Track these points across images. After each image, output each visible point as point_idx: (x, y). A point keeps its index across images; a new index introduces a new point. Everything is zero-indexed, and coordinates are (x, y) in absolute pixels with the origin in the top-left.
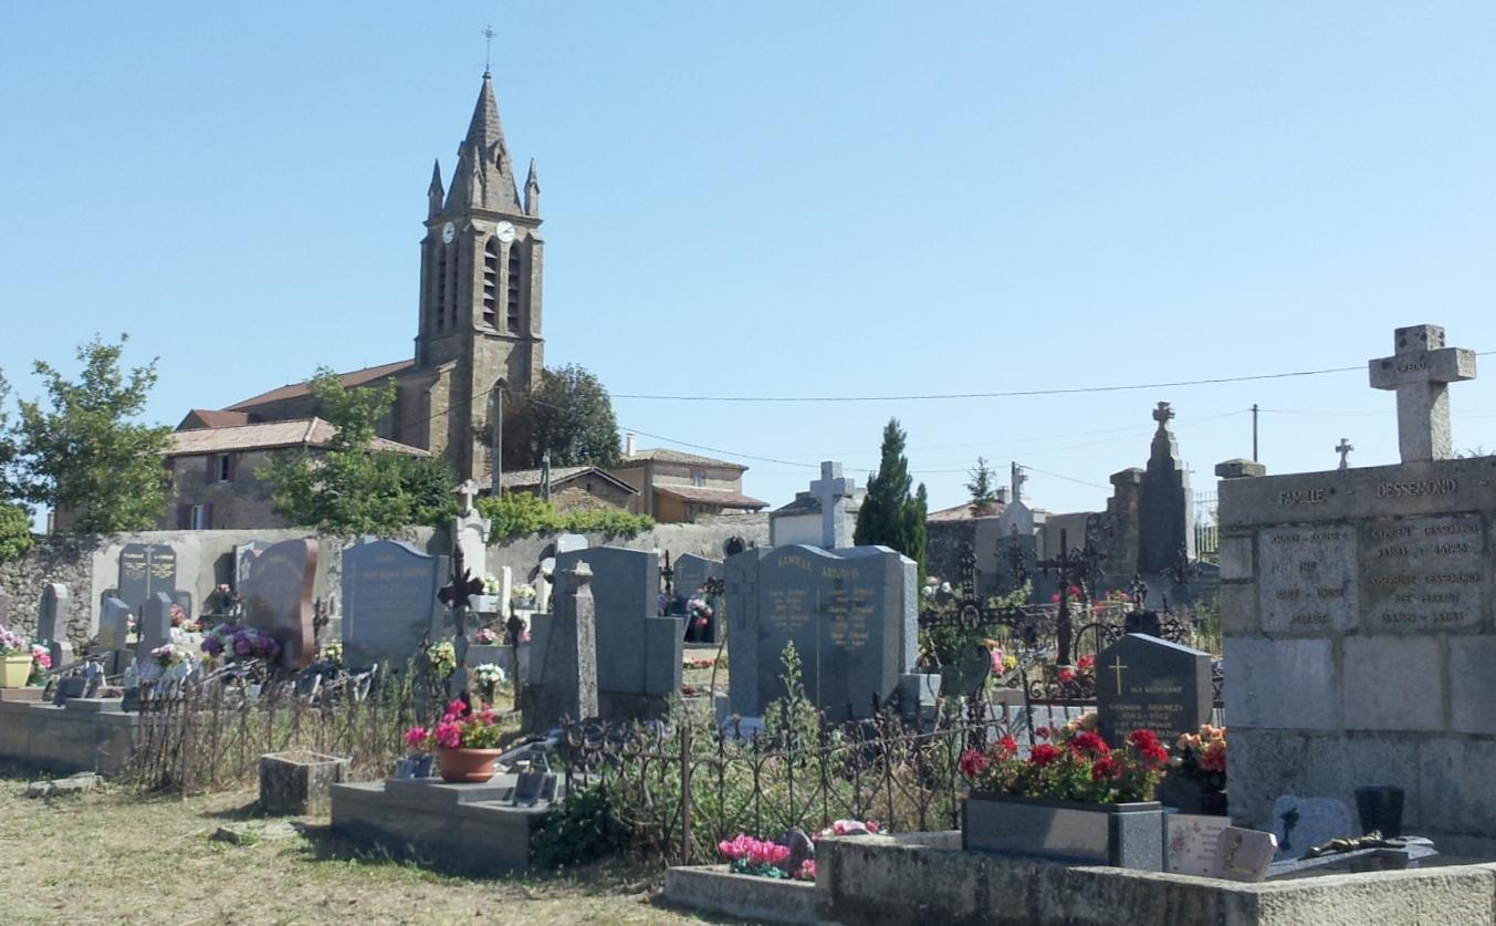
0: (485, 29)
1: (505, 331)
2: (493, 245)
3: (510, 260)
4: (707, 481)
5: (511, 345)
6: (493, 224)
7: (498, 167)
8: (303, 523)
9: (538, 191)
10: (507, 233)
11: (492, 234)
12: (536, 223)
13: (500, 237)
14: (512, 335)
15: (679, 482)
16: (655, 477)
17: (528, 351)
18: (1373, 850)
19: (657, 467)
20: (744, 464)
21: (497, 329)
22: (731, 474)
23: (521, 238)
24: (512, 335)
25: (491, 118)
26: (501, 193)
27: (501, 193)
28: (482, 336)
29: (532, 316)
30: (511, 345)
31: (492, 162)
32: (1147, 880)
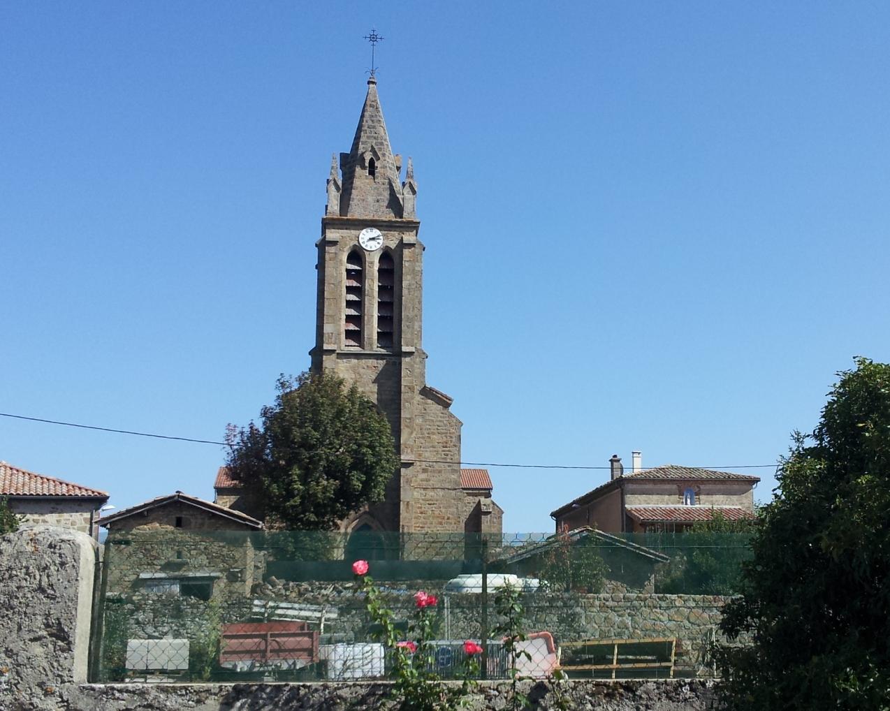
0: (380, 34)
1: (376, 348)
2: (357, 255)
3: (380, 271)
4: (702, 497)
5: (381, 364)
6: (354, 232)
7: (372, 173)
8: (175, 619)
9: (414, 192)
10: (372, 241)
11: (352, 243)
12: (413, 226)
13: (363, 246)
14: (383, 351)
15: (662, 502)
16: (628, 498)
17: (399, 365)
18: (631, 543)
19: (630, 486)
20: (753, 473)
21: (361, 345)
22: (736, 487)
23: (393, 245)
24: (383, 351)
25: (370, 123)
26: (370, 199)
27: (370, 199)
28: (334, 356)
29: (403, 328)
30: (381, 364)
31: (363, 167)
32: (575, 665)
